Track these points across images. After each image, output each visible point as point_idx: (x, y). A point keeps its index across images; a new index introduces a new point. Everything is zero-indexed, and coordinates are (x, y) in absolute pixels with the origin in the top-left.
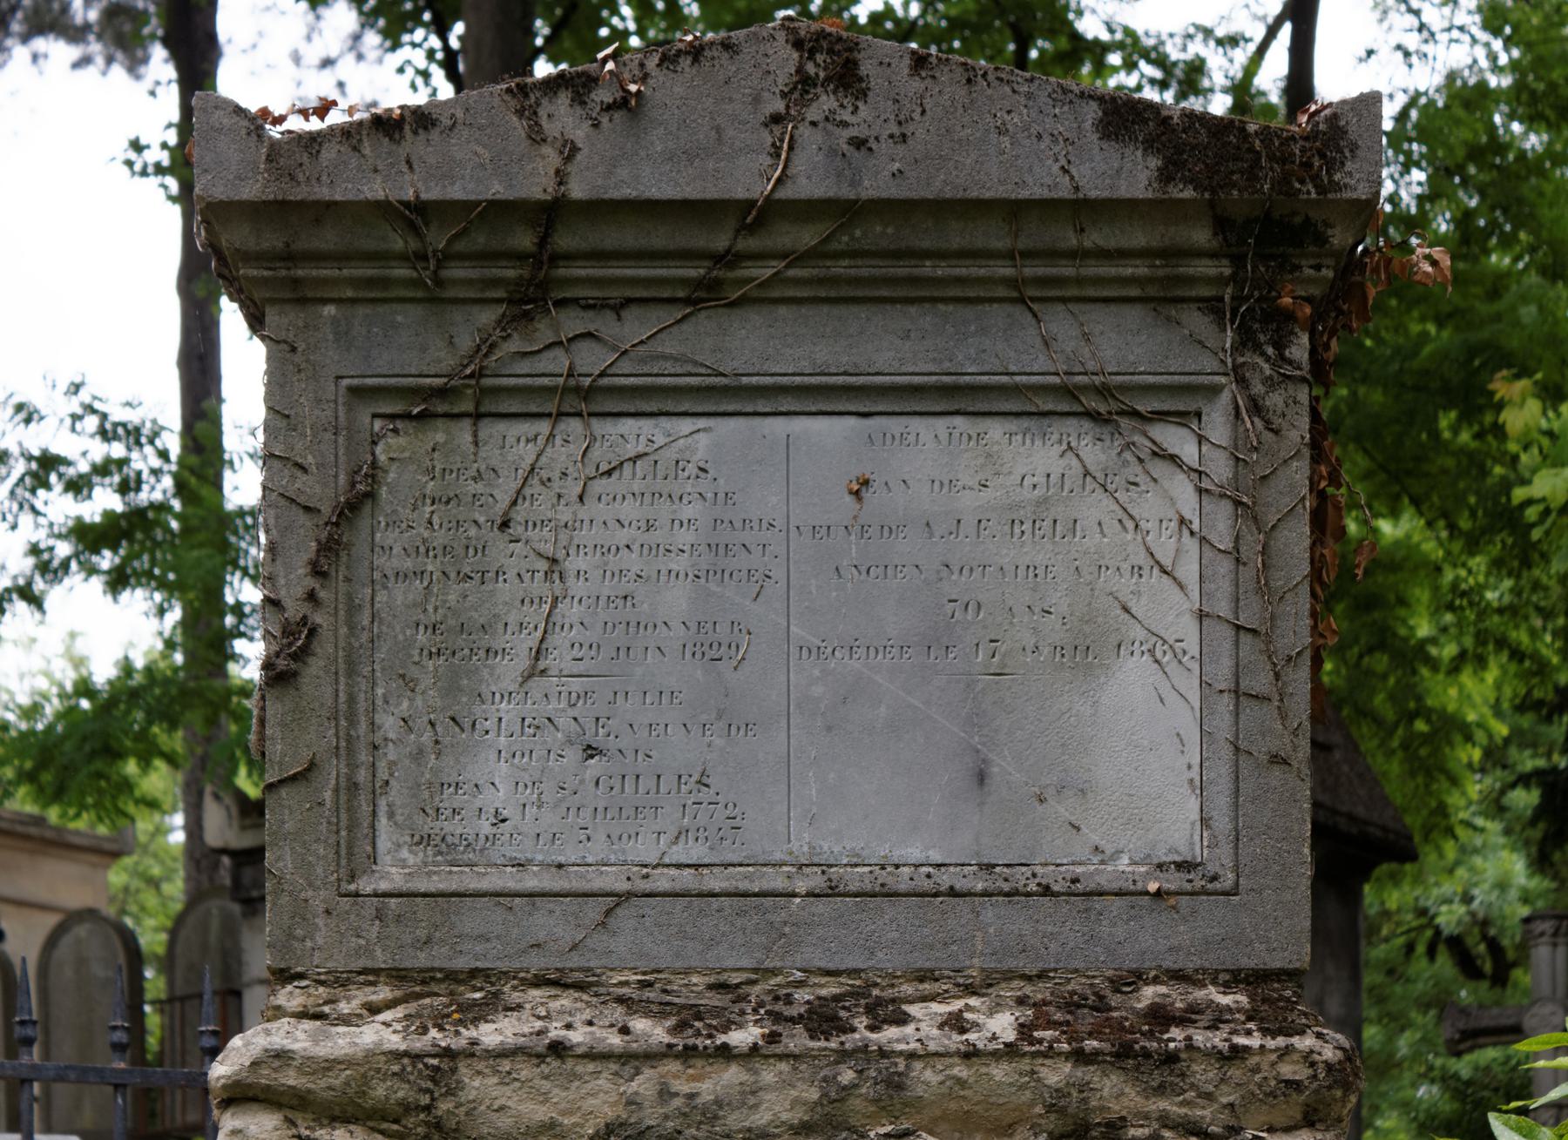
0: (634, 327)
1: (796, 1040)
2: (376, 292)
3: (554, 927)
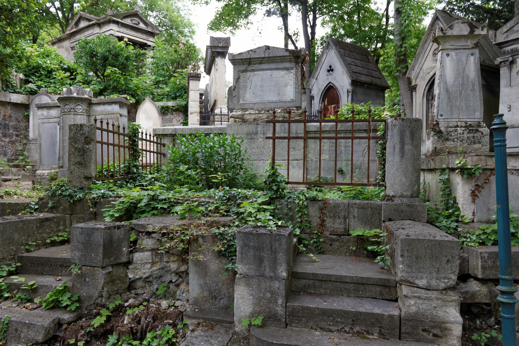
0: (256, 66)
1: (266, 112)
2: (240, 64)
3: (251, 105)
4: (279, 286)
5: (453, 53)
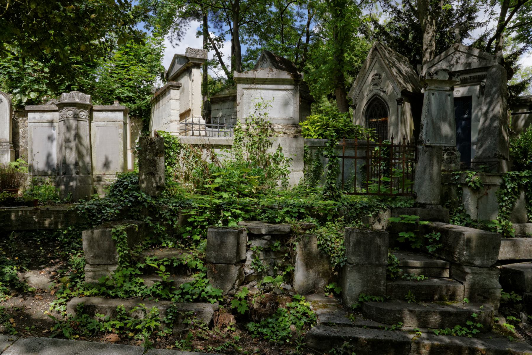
5: (436, 93)
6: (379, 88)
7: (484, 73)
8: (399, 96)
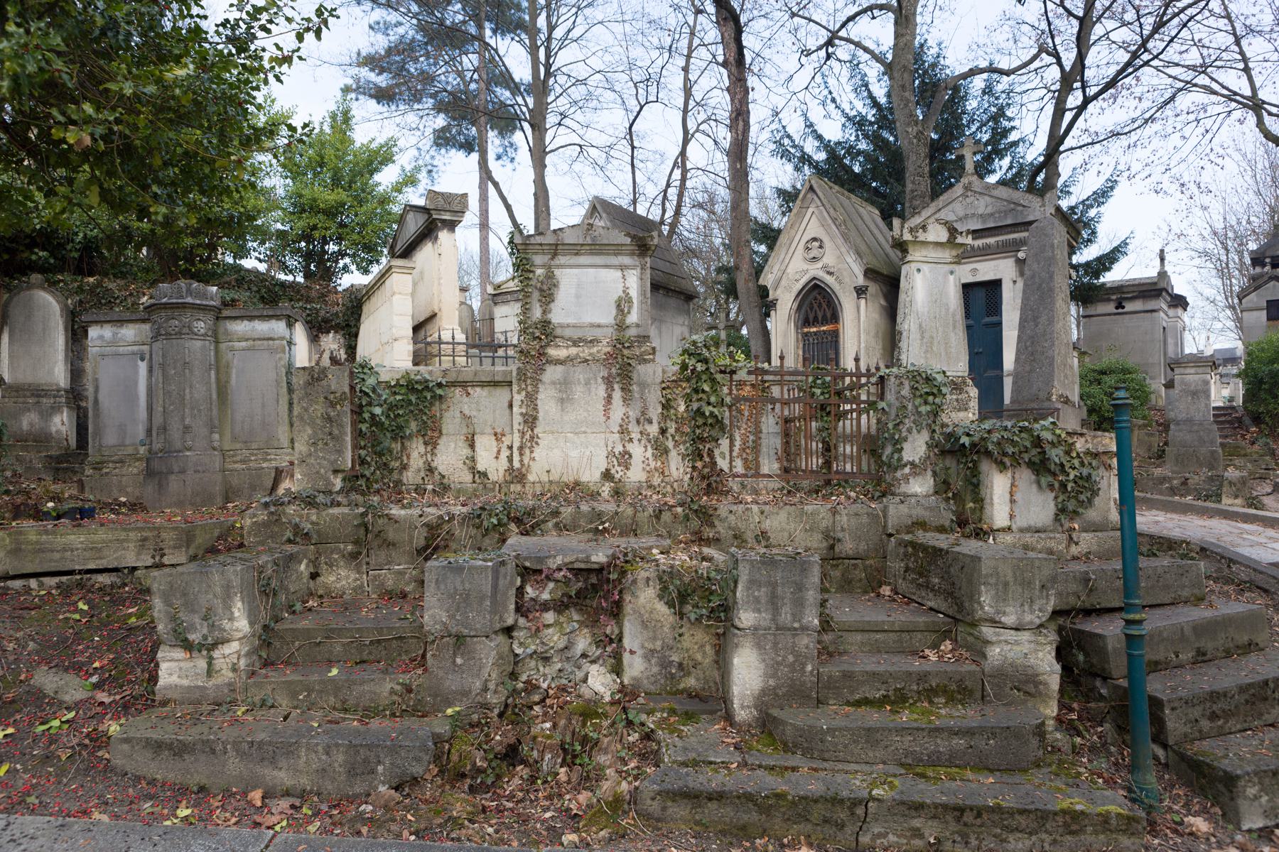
4: (806, 642)
6: (820, 265)
7: (1025, 234)
8: (861, 281)
